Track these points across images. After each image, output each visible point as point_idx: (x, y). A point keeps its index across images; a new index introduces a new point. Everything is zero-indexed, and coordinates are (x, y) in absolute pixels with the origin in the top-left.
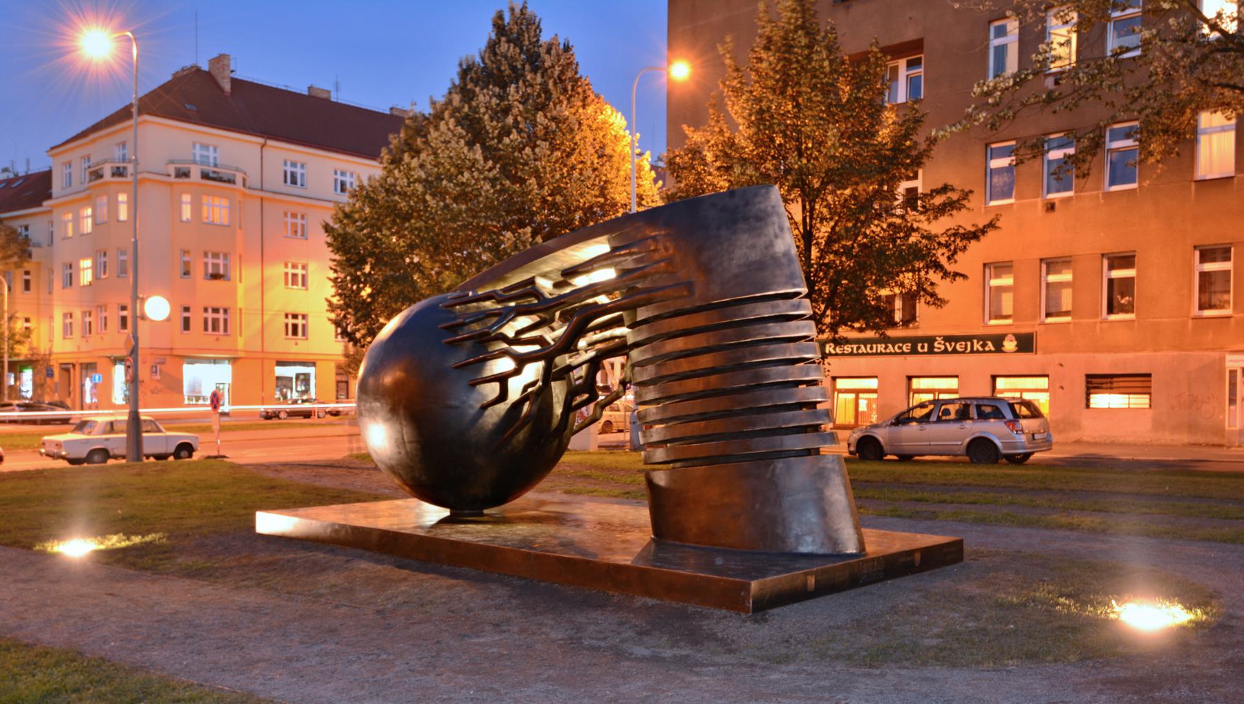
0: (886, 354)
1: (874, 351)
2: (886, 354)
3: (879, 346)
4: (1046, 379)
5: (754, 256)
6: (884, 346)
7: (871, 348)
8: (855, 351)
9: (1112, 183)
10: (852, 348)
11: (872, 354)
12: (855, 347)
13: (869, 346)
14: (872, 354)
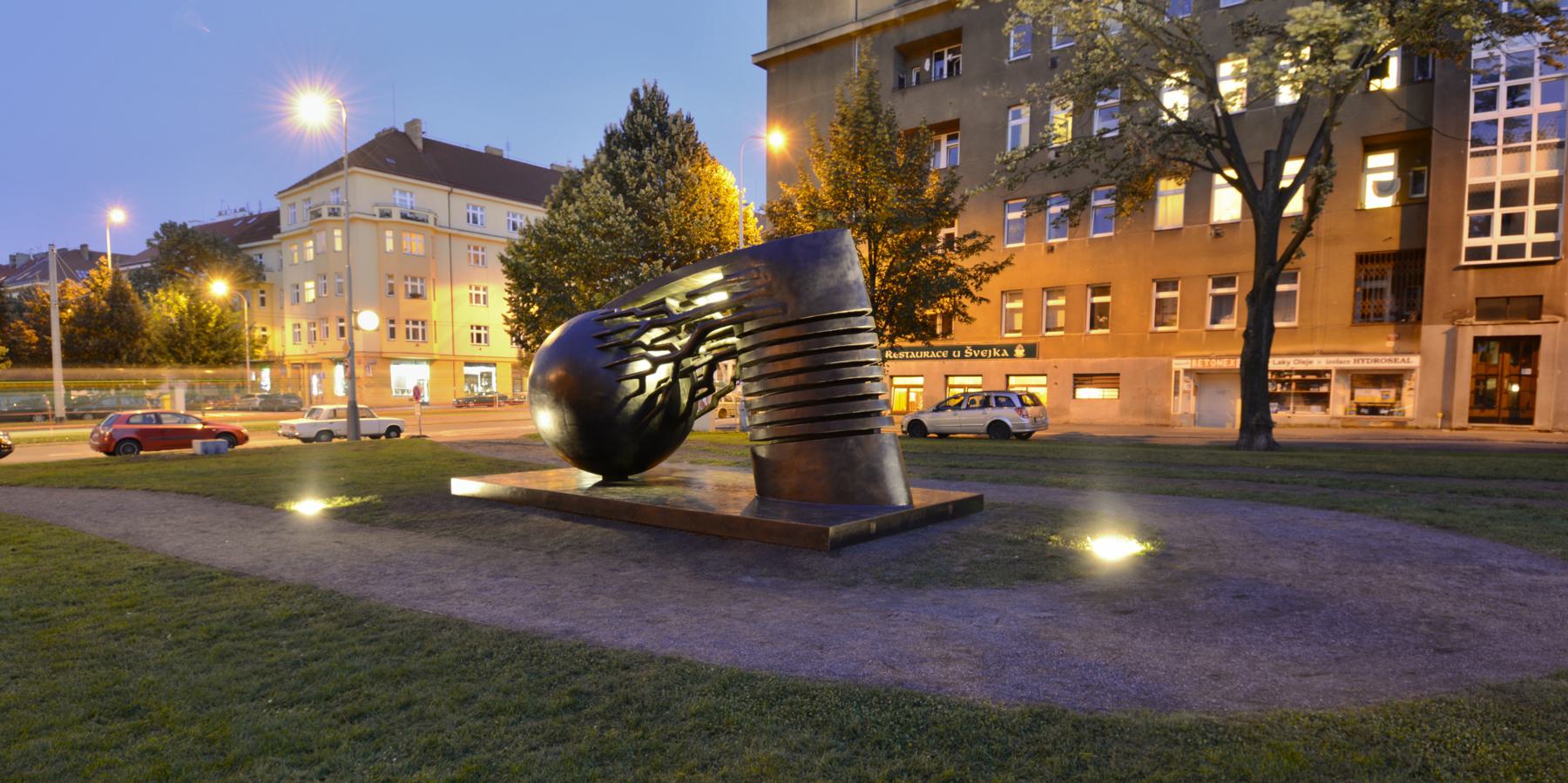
4: (1045, 378)
5: (832, 283)
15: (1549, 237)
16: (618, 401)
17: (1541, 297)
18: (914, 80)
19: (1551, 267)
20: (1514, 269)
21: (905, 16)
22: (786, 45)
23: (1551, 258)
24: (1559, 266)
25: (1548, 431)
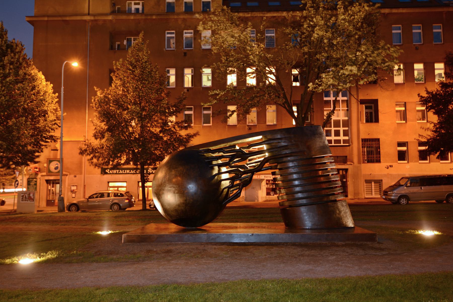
0: (130, 173)
1: (125, 172)
2: (130, 173)
3: (127, 171)
4: (126, 183)
5: (321, 144)
6: (129, 171)
7: (124, 172)
8: (118, 172)
9: (204, 123)
10: (117, 171)
11: (125, 174)
12: (118, 171)
13: (123, 171)
14: (125, 174)
15: (347, 138)
16: (221, 190)
17: (346, 157)
18: (117, 47)
19: (348, 147)
20: (339, 147)
21: (116, 20)
22: (48, 16)
23: (348, 144)
24: (350, 147)
25: (353, 199)
